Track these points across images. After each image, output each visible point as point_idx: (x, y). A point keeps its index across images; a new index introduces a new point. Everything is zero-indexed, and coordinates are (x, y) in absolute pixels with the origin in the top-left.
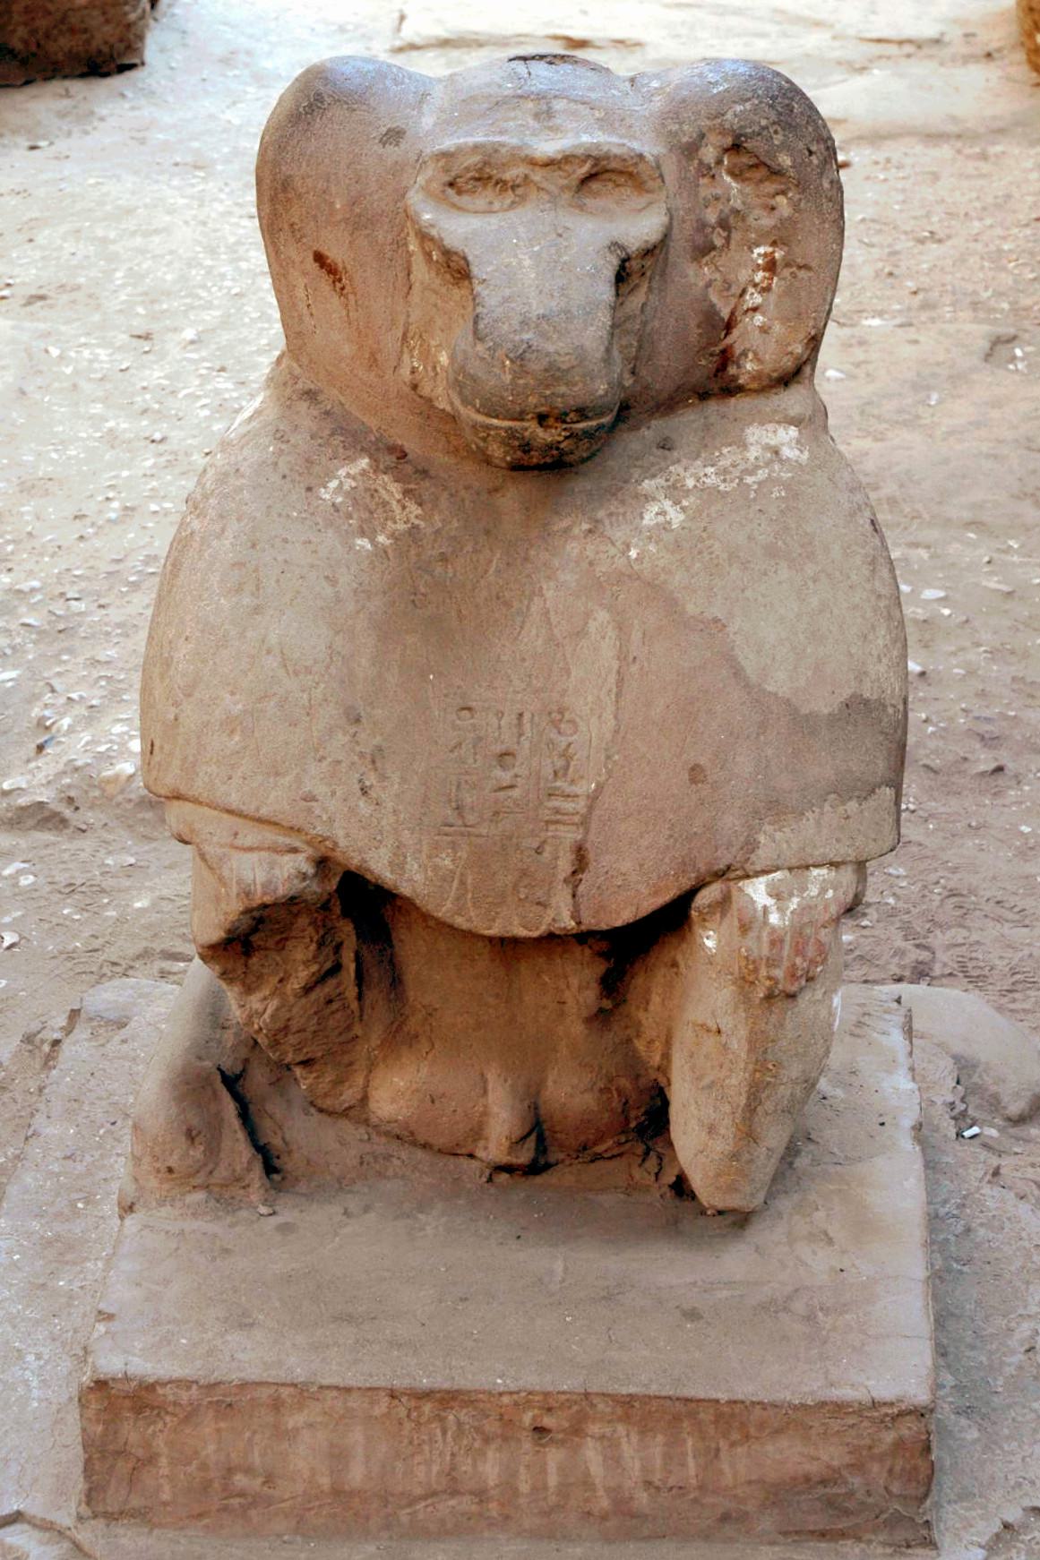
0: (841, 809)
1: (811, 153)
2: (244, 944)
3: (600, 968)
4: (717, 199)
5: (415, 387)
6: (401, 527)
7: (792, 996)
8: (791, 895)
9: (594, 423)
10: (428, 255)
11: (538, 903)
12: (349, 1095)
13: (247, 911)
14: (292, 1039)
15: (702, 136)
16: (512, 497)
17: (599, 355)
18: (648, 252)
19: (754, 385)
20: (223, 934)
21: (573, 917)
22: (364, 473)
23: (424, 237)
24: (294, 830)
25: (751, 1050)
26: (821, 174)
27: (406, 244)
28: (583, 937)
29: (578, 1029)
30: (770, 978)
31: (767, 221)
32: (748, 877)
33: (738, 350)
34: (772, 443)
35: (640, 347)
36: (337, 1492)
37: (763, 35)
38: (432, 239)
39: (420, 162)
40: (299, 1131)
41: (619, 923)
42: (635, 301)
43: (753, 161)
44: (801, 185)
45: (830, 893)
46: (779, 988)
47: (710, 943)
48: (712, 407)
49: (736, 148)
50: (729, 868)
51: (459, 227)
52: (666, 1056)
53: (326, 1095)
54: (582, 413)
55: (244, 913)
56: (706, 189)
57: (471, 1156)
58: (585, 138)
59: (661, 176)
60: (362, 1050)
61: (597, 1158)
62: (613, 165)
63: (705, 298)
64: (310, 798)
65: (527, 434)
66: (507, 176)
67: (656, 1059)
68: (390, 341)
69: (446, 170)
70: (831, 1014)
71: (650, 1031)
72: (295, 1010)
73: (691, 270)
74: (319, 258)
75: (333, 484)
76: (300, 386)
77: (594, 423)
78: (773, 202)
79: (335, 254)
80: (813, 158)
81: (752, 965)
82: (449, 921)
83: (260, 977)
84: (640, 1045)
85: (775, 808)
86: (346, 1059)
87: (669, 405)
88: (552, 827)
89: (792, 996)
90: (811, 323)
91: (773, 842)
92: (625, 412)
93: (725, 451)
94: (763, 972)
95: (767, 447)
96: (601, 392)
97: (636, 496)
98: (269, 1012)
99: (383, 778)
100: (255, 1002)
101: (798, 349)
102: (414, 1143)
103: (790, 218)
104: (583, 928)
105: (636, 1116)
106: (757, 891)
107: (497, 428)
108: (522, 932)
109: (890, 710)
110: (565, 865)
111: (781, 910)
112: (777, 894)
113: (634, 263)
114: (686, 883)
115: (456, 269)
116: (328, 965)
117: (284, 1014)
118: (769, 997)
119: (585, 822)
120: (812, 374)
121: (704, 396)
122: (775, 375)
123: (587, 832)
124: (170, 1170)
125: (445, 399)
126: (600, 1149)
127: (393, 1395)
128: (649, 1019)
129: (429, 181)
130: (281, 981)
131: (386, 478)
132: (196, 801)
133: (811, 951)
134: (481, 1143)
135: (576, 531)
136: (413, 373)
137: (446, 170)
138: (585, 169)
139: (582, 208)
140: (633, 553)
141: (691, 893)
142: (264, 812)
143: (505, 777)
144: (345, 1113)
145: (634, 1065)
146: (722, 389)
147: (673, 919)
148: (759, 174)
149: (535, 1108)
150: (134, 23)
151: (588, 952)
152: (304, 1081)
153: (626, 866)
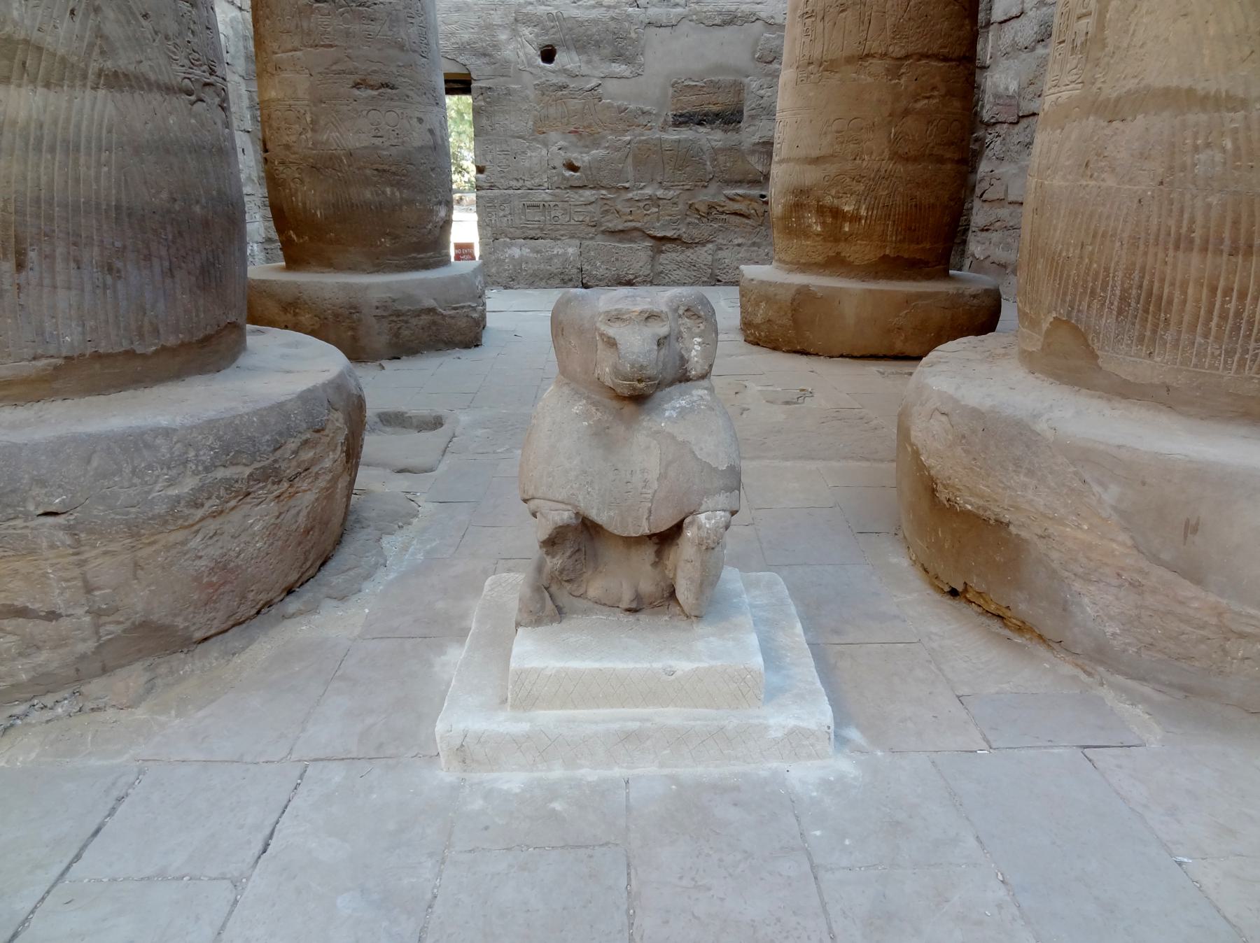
2: (552, 543)
3: (656, 548)
12: (582, 591)
16: (629, 408)
23: (602, 335)
28: (650, 537)
31: (697, 331)
37: (1156, 254)
39: (600, 314)
40: (564, 599)
42: (662, 352)
46: (709, 547)
51: (612, 331)
60: (585, 576)
71: (670, 567)
81: (701, 539)
85: (707, 493)
87: (671, 384)
91: (708, 503)
92: (660, 385)
100: (555, 561)
105: (666, 594)
106: (702, 517)
112: (708, 518)
115: (612, 343)
128: (669, 564)
142: (560, 498)
147: (678, 529)
152: (568, 586)
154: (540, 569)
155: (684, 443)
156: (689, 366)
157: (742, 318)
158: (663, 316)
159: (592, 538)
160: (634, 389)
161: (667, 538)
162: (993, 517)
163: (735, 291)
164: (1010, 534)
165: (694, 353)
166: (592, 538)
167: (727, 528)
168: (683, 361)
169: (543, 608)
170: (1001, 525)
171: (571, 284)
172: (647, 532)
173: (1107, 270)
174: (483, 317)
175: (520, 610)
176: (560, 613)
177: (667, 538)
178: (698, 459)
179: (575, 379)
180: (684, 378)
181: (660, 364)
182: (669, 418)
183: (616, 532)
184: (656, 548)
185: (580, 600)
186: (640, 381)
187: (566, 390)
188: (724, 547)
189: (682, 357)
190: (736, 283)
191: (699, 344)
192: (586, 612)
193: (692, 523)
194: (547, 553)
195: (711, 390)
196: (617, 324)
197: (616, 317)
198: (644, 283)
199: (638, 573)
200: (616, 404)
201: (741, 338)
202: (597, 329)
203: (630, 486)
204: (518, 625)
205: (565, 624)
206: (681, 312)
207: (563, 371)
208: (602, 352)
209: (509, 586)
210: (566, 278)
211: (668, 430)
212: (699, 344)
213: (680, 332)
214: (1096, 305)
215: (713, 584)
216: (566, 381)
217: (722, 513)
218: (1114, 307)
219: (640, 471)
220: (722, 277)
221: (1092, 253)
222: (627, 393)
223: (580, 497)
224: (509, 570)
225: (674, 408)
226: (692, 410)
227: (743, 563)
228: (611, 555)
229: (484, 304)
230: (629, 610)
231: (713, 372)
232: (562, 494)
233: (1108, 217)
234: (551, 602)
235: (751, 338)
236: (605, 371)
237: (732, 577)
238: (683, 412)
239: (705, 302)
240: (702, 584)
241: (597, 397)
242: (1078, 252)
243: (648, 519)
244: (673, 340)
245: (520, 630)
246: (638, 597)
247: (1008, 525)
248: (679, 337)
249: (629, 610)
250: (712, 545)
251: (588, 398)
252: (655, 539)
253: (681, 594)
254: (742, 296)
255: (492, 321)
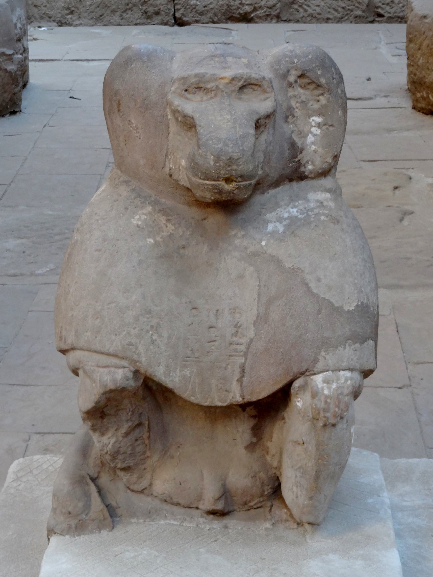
0: (353, 347)
1: (333, 78)
2: (100, 414)
3: (252, 422)
4: (295, 96)
5: (171, 176)
6: (165, 234)
7: (334, 425)
8: (333, 382)
9: (248, 183)
10: (177, 119)
11: (227, 391)
12: (145, 483)
13: (105, 393)
14: (120, 457)
15: (288, 71)
16: (215, 219)
17: (249, 153)
18: (268, 116)
19: (312, 175)
20: (93, 404)
21: (241, 396)
22: (150, 213)
23: (175, 112)
25: (317, 449)
26: (337, 88)
27: (167, 116)
28: (244, 406)
29: (242, 451)
30: (325, 417)
31: (316, 106)
32: (315, 374)
33: (303, 162)
34: (320, 199)
35: (265, 157)
38: (179, 112)
39: (173, 81)
40: (120, 496)
41: (261, 397)
42: (264, 137)
43: (310, 81)
44: (329, 91)
45: (349, 382)
46: (330, 421)
47: (299, 404)
48: (295, 185)
49: (301, 76)
50: (307, 370)
51: (190, 106)
52: (280, 462)
53: (135, 483)
54: (243, 177)
55: (103, 394)
56: (291, 92)
57: (197, 508)
58: (240, 71)
59: (272, 86)
60: (149, 462)
61: (252, 508)
62: (252, 82)
63: (291, 137)
65: (220, 187)
66: (209, 86)
67: (275, 464)
69: (183, 84)
70: (351, 435)
72: (122, 444)
73: (285, 126)
75: (137, 217)
76: (121, 179)
77: (248, 183)
78: (318, 98)
80: (334, 80)
82: (188, 399)
83: (107, 429)
84: (268, 458)
85: (326, 344)
86: (143, 467)
87: (277, 184)
88: (231, 358)
89: (334, 425)
90: (335, 150)
91: (328, 358)
92: (259, 186)
93: (300, 202)
94: (322, 414)
95: (318, 201)
96: (251, 169)
97: (264, 220)
98: (111, 444)
99: (160, 336)
100: (105, 439)
101: (329, 160)
102: (172, 504)
103: (325, 105)
104: (245, 400)
105: (268, 490)
106: (318, 379)
107: (208, 185)
108: (219, 404)
109: (372, 309)
111: (329, 388)
112: (327, 381)
113: (262, 120)
114: (289, 378)
115: (189, 124)
116: (137, 422)
117: (117, 445)
118: (325, 425)
120: (335, 173)
121: (291, 180)
122: (320, 171)
123: (246, 359)
124: (70, 513)
125: (183, 178)
126: (252, 504)
128: (272, 446)
129: (176, 89)
130: (116, 430)
131: (159, 214)
133: (342, 406)
134: (202, 502)
135: (239, 235)
136: (170, 169)
137: (183, 84)
138: (241, 83)
139: (240, 99)
140: (263, 243)
141: (289, 384)
142: (111, 350)
144: (142, 492)
145: (265, 466)
146: (298, 177)
148: (312, 86)
149: (224, 485)
150: (17, 93)
151: (246, 415)
152: (125, 477)
154: (85, 450)
155: (294, 271)
156: (303, 157)
157: (410, 73)
158: (265, 84)
159: (159, 407)
160: (220, 192)
161: (270, 408)
163: (400, 31)
165: (310, 139)
166: (159, 407)
167: (356, 395)
168: (295, 150)
169: (87, 507)
171: (159, 18)
172: (239, 399)
174: (24, 70)
175: (54, 510)
176: (112, 515)
177: (270, 408)
178: (313, 295)
179: (139, 176)
180: (296, 174)
181: (260, 156)
182: (273, 233)
183: (193, 399)
184: (252, 422)
185: (142, 496)
186: (228, 180)
187: (124, 191)
188: (351, 423)
189: (293, 145)
190: (402, 19)
191: (319, 125)
192: (150, 515)
193: (303, 388)
194: (94, 428)
195: (336, 192)
196: (198, 97)
197: (197, 87)
198: (267, 18)
199: (230, 460)
200: (195, 213)
201: (407, 104)
202: (169, 104)
203: (213, 333)
204: (51, 532)
205: (119, 532)
206: (292, 79)
207: (120, 163)
208: (176, 135)
209: (42, 474)
210: (151, 10)
211: (270, 251)
212: (319, 125)
213: (290, 108)
215: (335, 477)
216: (124, 177)
217: (348, 374)
219: (232, 309)
220: (385, 10)
222: (209, 196)
223: (141, 349)
224: (46, 450)
225: (280, 220)
226: (306, 222)
227: (386, 444)
228: (188, 432)
229: (25, 50)
230: (213, 513)
231: (339, 168)
232: (115, 344)
234: (97, 499)
235: (422, 105)
236: (179, 163)
237: (365, 465)
238: (293, 225)
239: (327, 64)
240: (317, 477)
241: (167, 202)
243: (240, 380)
244: (279, 117)
245: (54, 539)
246: (225, 494)
248: (289, 114)
249: (213, 513)
250: (332, 421)
251: (155, 203)
252: (251, 411)
253: (287, 492)
254: (410, 41)
255: (37, 75)
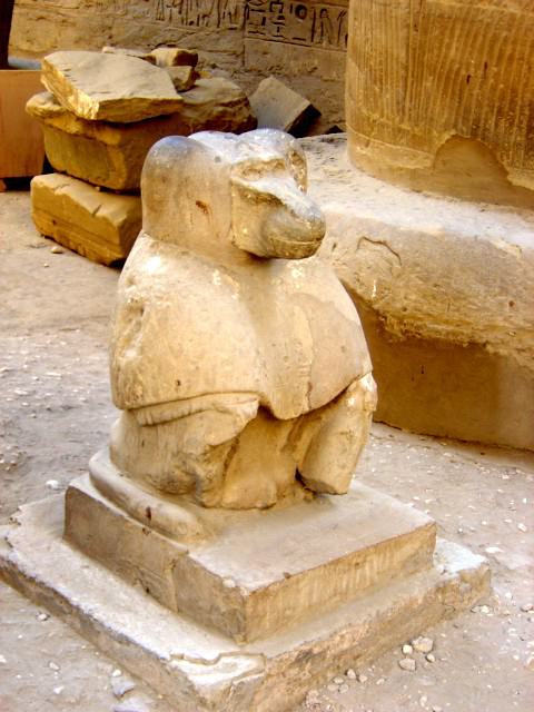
12: (217, 498)
16: (257, 274)
24: (256, 392)
36: (310, 606)
64: (258, 380)
68: (225, 228)
74: (199, 204)
79: (205, 200)
110: (305, 390)
119: (309, 375)
127: (325, 566)
132: (219, 393)
143: (287, 364)
153: (325, 384)
162: (467, 340)
164: (487, 353)
170: (476, 347)
173: (514, 91)
214: (503, 123)
218: (524, 125)
221: (498, 74)
233: (514, 42)
242: (480, 72)
243: (308, 394)
247: (484, 345)
